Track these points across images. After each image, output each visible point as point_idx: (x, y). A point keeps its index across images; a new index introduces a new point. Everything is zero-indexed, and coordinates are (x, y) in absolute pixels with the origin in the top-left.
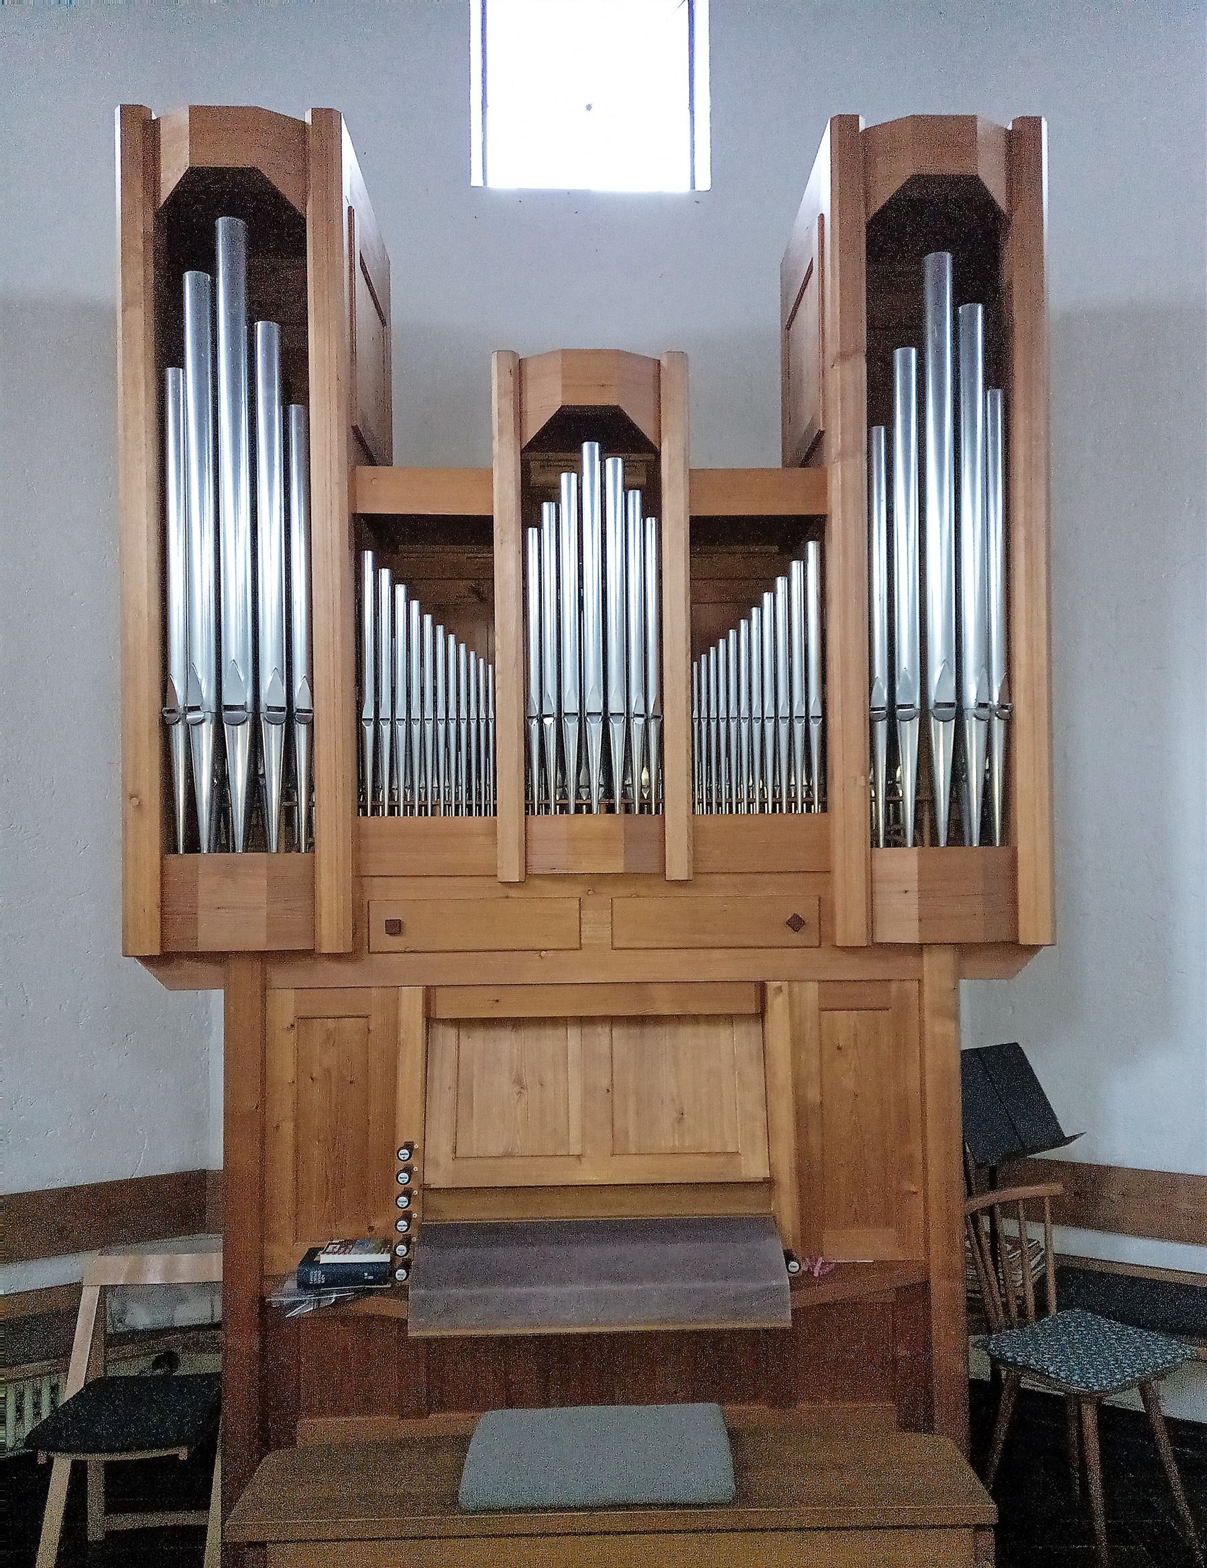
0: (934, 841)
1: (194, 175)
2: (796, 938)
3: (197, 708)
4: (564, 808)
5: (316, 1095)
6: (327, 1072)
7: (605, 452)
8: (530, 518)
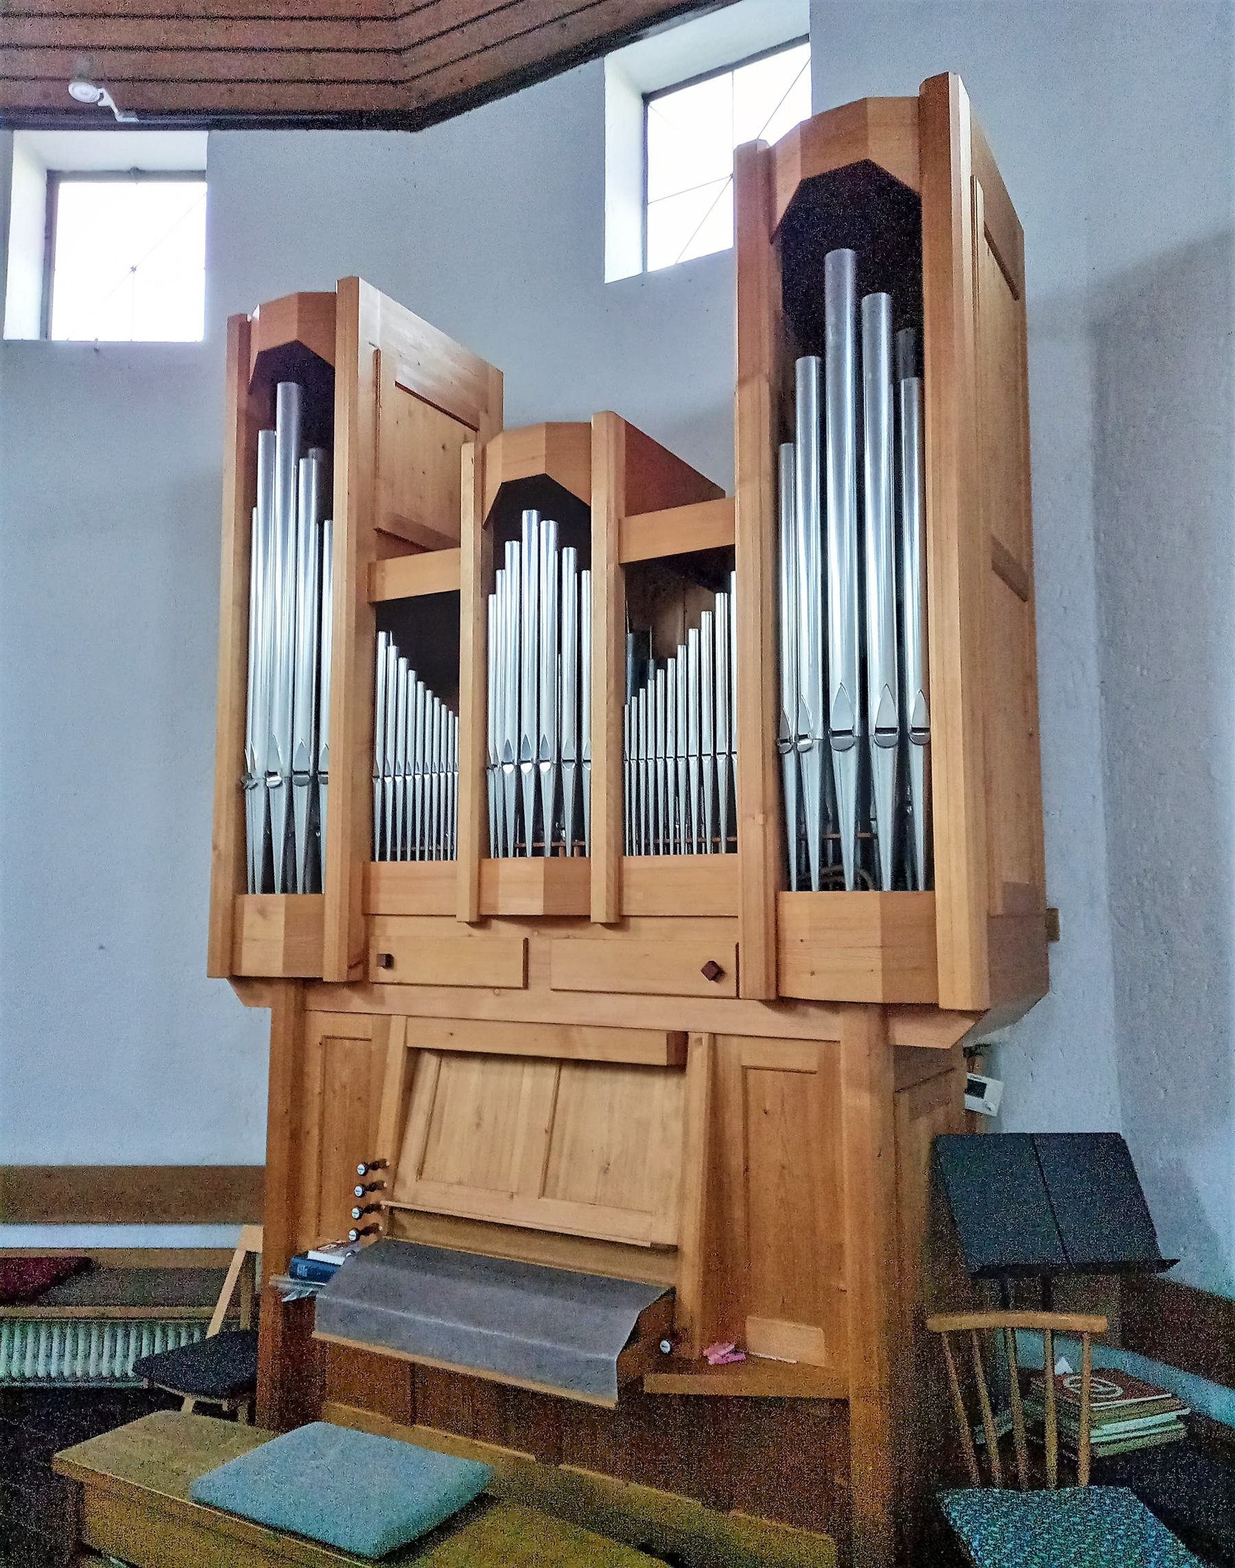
0: (294, 890)
1: (807, 187)
2: (712, 987)
3: (805, 737)
4: (538, 852)
5: (335, 1107)
6: (344, 1087)
7: (541, 518)
8: (489, 587)
